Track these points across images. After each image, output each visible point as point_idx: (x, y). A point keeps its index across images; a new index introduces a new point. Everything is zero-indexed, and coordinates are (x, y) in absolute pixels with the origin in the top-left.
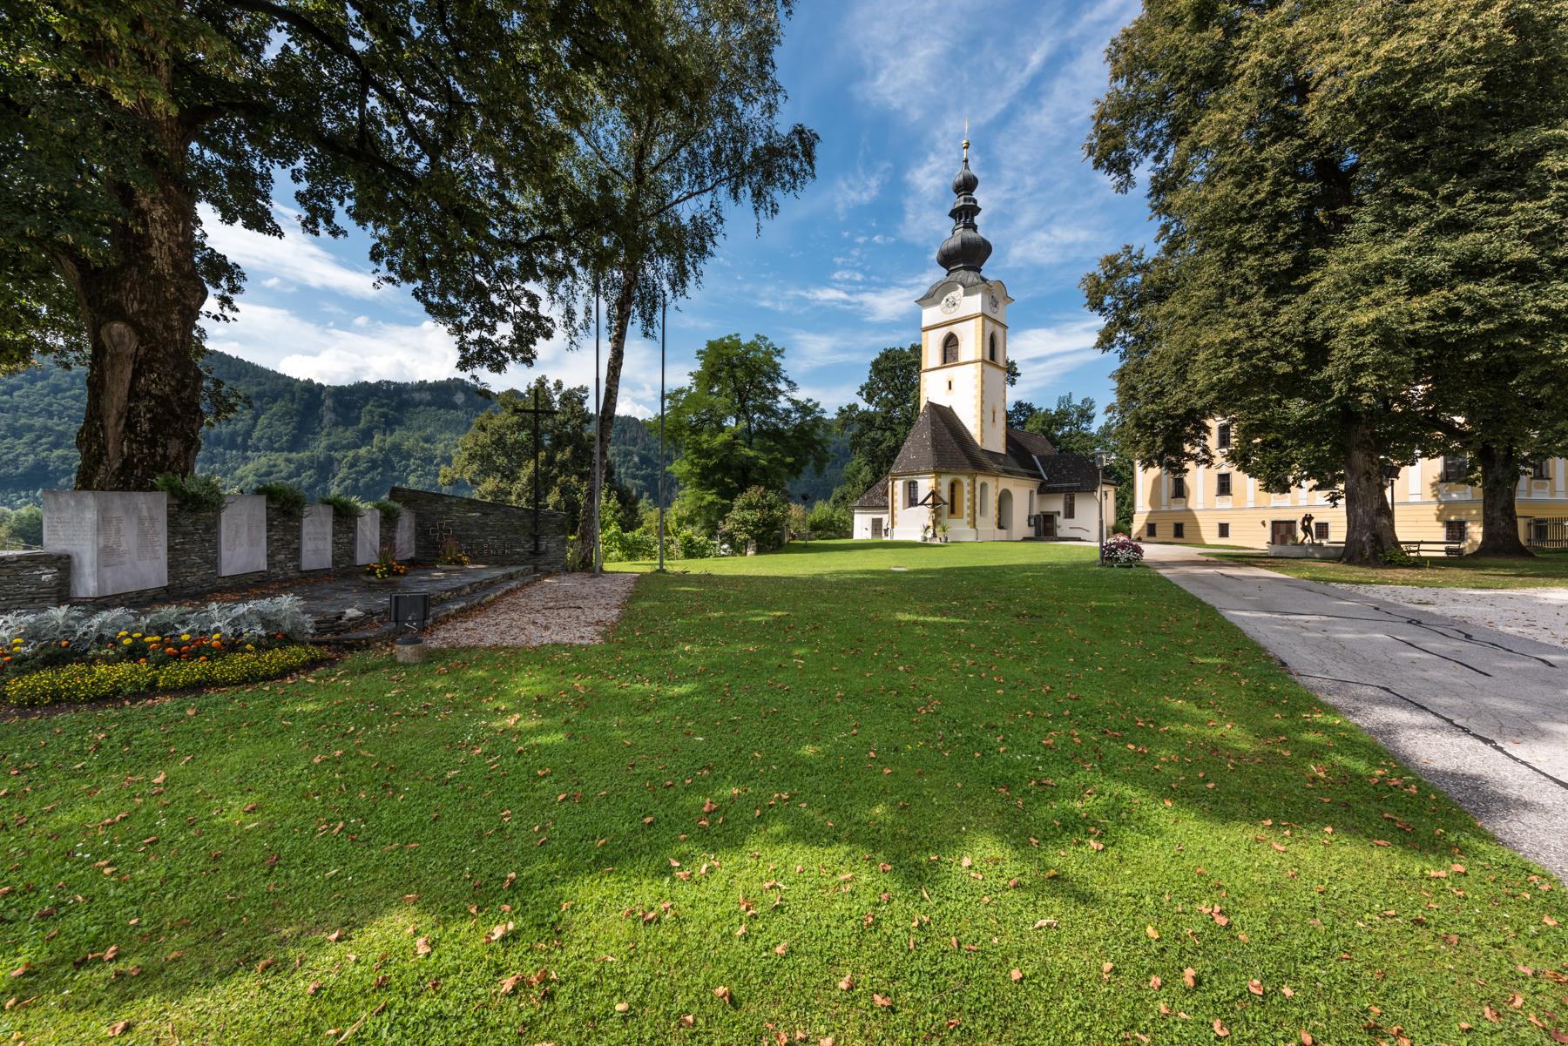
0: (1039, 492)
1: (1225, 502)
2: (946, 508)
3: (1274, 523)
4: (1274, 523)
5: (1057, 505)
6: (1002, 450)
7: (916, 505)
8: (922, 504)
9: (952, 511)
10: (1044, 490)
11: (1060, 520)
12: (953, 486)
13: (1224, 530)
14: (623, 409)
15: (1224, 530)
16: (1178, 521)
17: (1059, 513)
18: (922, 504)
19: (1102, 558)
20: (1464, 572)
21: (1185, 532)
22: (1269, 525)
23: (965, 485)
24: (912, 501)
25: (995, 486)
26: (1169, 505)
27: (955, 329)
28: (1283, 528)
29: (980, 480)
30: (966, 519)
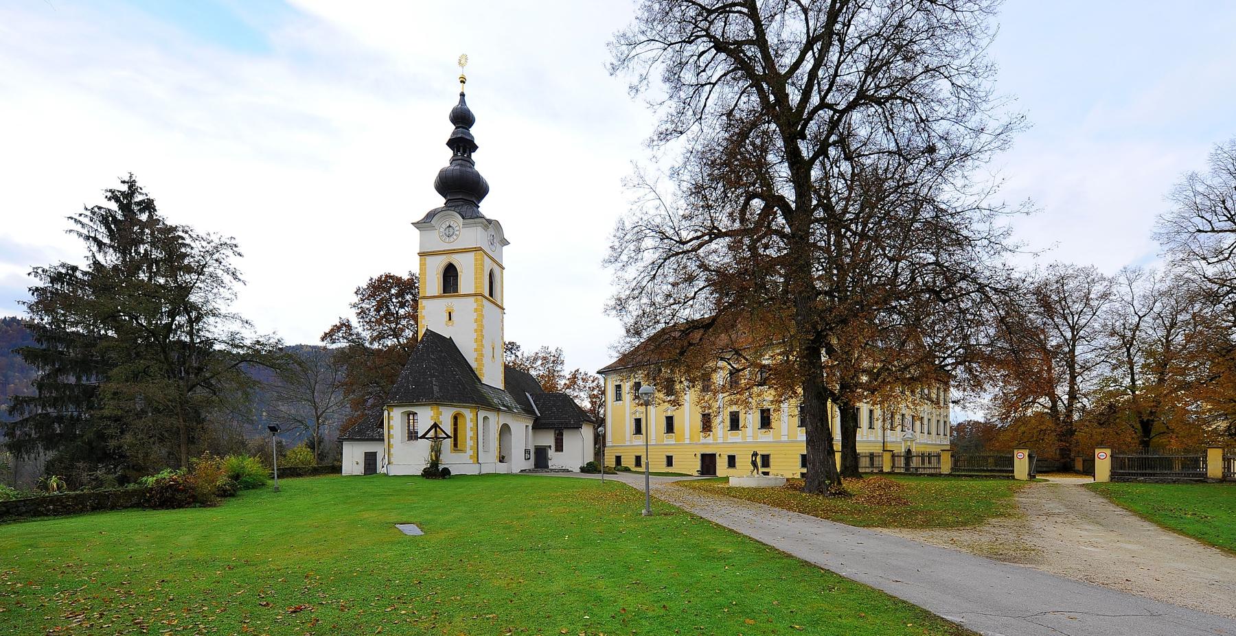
0: (533, 428)
1: (670, 440)
2: (448, 443)
3: (703, 456)
4: (703, 456)
5: (548, 439)
6: (501, 387)
7: (417, 438)
8: (423, 437)
9: (456, 445)
10: (538, 426)
11: (551, 453)
12: (455, 418)
13: (669, 461)
14: (715, 52)
15: (669, 461)
16: (638, 454)
17: (550, 447)
18: (423, 437)
19: (1206, 452)
20: (644, 484)
21: (665, 460)
22: (699, 457)
23: (468, 420)
24: (412, 436)
25: (496, 421)
26: (724, 437)
27: (457, 260)
28: (707, 459)
29: (482, 414)
30: (470, 452)
